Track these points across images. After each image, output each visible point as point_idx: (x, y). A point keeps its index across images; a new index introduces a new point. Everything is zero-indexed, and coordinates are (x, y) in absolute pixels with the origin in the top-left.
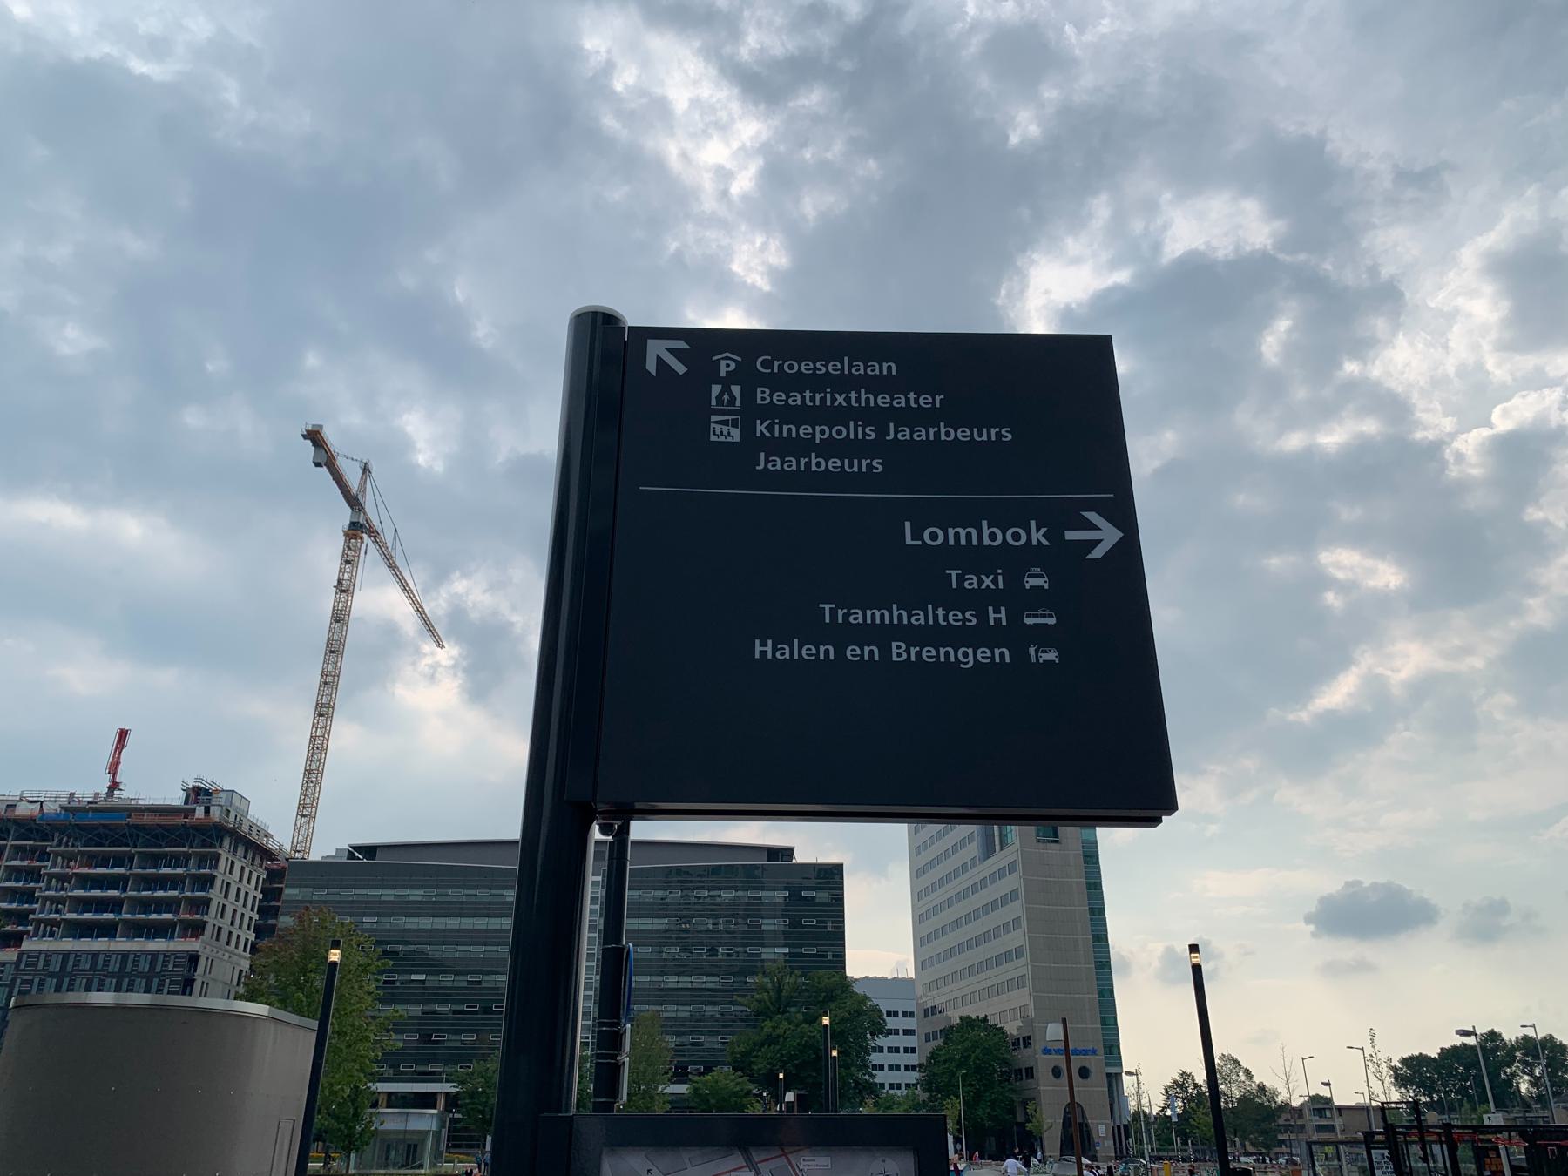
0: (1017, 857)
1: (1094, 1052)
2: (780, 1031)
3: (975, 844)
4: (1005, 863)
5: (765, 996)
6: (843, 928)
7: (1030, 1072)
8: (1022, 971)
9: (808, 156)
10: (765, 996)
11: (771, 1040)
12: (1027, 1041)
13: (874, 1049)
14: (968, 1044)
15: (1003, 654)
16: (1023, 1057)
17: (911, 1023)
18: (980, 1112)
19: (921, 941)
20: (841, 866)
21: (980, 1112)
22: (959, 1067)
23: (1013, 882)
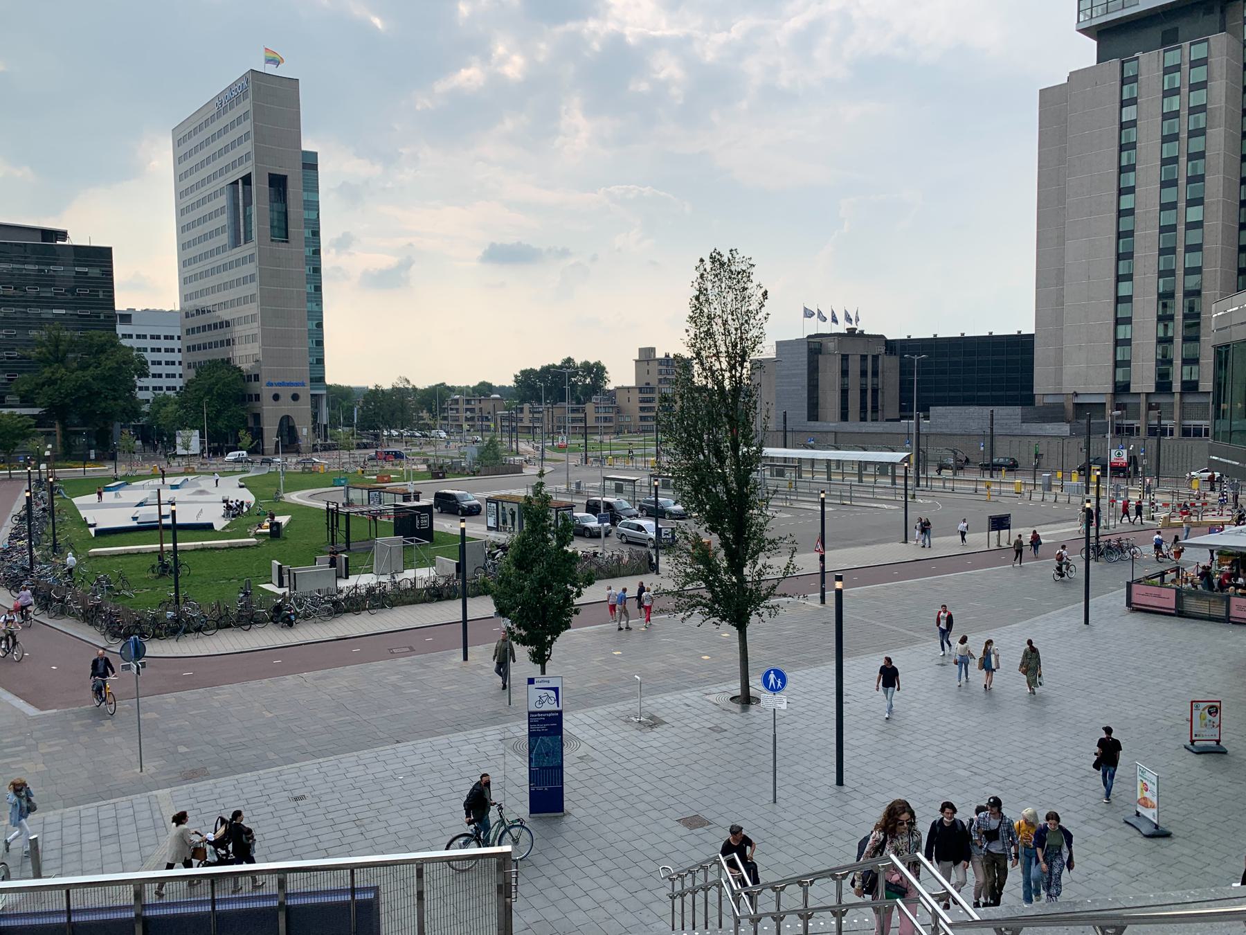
0: (255, 251)
1: (303, 385)
2: (58, 375)
3: (225, 216)
4: (247, 253)
5: (44, 350)
6: (112, 296)
7: (258, 397)
8: (256, 331)
9: (543, 46)
10: (44, 350)
11: (51, 382)
12: (257, 378)
13: (141, 388)
14: (213, 380)
15: (64, 919)
16: (254, 387)
17: (176, 344)
18: (219, 424)
19: (185, 281)
20: (110, 249)
21: (219, 424)
22: (206, 394)
23: (251, 268)
